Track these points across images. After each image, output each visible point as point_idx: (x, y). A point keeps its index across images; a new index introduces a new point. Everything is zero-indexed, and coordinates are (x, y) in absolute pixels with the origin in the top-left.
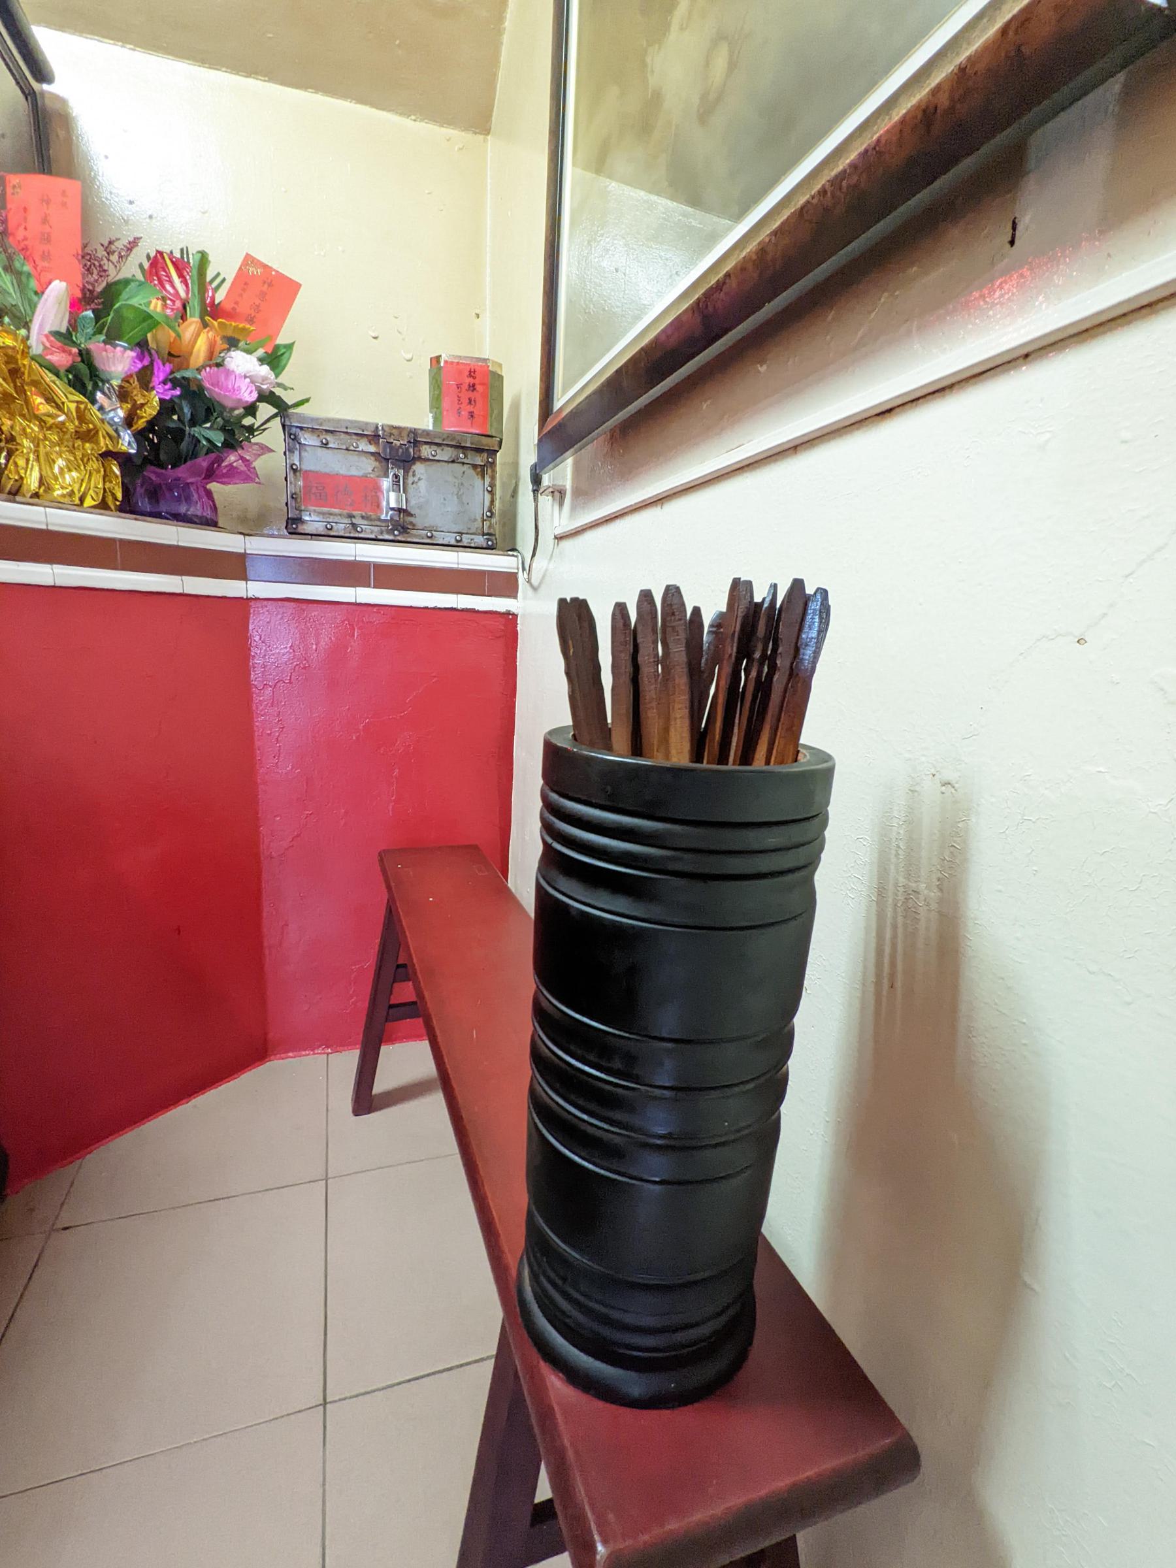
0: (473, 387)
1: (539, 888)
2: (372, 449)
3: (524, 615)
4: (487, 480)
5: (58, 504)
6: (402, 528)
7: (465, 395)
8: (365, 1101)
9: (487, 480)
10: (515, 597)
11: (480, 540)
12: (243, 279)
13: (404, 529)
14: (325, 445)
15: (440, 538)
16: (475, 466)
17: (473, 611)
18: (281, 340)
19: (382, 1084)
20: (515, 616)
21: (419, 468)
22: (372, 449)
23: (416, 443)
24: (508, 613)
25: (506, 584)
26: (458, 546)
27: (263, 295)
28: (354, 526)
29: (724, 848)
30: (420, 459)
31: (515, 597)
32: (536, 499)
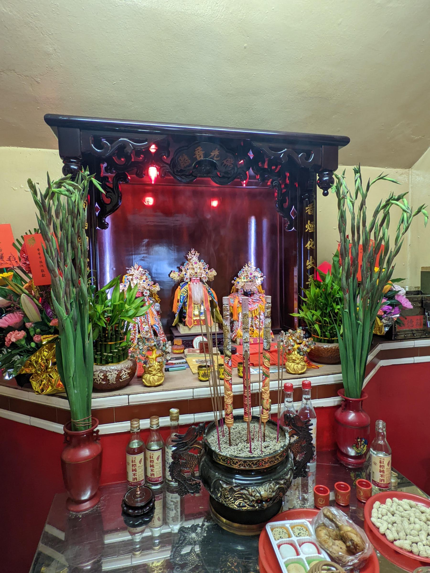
28: (414, 334)
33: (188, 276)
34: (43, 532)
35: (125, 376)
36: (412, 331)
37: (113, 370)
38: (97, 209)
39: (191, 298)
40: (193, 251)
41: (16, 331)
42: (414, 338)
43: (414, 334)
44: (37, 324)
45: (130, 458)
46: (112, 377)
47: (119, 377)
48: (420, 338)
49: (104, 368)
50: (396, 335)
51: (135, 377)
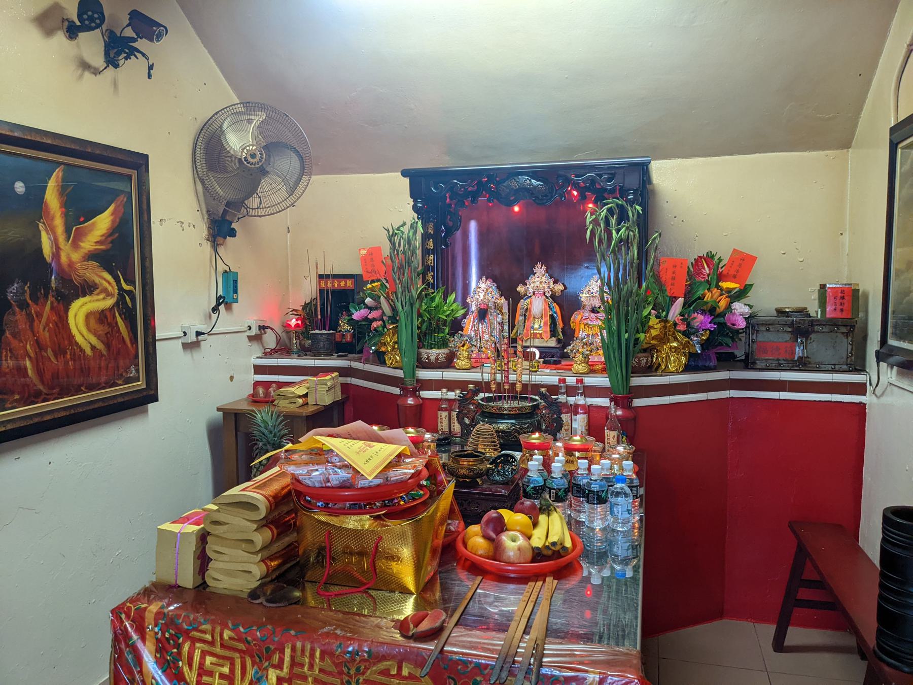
0: (843, 298)
1: (879, 604)
2: (790, 330)
3: (870, 405)
4: (850, 339)
5: (672, 373)
6: (803, 365)
7: (838, 301)
8: (779, 645)
9: (850, 339)
10: (865, 395)
11: (845, 367)
12: (732, 260)
13: (805, 364)
14: (768, 330)
15: (823, 367)
16: (843, 333)
17: (841, 402)
18: (748, 282)
19: (788, 642)
20: (865, 405)
21: (813, 336)
22: (790, 330)
23: (812, 325)
24: (861, 403)
25: (860, 389)
26: (833, 371)
27: (740, 265)
28: (780, 364)
29: (235, 470)
30: (813, 332)
31: (865, 395)
32: (878, 366)
33: (531, 290)
34: (410, 540)
35: (442, 358)
36: (778, 360)
37: (433, 353)
38: (443, 231)
39: (530, 311)
40: (539, 265)
41: (549, 580)
42: (779, 368)
43: (780, 364)
44: (389, 317)
45: (440, 413)
46: (433, 358)
47: (437, 359)
48: (790, 370)
49: (428, 351)
50: (754, 363)
51: (449, 363)
